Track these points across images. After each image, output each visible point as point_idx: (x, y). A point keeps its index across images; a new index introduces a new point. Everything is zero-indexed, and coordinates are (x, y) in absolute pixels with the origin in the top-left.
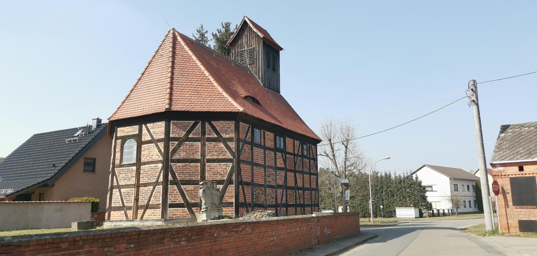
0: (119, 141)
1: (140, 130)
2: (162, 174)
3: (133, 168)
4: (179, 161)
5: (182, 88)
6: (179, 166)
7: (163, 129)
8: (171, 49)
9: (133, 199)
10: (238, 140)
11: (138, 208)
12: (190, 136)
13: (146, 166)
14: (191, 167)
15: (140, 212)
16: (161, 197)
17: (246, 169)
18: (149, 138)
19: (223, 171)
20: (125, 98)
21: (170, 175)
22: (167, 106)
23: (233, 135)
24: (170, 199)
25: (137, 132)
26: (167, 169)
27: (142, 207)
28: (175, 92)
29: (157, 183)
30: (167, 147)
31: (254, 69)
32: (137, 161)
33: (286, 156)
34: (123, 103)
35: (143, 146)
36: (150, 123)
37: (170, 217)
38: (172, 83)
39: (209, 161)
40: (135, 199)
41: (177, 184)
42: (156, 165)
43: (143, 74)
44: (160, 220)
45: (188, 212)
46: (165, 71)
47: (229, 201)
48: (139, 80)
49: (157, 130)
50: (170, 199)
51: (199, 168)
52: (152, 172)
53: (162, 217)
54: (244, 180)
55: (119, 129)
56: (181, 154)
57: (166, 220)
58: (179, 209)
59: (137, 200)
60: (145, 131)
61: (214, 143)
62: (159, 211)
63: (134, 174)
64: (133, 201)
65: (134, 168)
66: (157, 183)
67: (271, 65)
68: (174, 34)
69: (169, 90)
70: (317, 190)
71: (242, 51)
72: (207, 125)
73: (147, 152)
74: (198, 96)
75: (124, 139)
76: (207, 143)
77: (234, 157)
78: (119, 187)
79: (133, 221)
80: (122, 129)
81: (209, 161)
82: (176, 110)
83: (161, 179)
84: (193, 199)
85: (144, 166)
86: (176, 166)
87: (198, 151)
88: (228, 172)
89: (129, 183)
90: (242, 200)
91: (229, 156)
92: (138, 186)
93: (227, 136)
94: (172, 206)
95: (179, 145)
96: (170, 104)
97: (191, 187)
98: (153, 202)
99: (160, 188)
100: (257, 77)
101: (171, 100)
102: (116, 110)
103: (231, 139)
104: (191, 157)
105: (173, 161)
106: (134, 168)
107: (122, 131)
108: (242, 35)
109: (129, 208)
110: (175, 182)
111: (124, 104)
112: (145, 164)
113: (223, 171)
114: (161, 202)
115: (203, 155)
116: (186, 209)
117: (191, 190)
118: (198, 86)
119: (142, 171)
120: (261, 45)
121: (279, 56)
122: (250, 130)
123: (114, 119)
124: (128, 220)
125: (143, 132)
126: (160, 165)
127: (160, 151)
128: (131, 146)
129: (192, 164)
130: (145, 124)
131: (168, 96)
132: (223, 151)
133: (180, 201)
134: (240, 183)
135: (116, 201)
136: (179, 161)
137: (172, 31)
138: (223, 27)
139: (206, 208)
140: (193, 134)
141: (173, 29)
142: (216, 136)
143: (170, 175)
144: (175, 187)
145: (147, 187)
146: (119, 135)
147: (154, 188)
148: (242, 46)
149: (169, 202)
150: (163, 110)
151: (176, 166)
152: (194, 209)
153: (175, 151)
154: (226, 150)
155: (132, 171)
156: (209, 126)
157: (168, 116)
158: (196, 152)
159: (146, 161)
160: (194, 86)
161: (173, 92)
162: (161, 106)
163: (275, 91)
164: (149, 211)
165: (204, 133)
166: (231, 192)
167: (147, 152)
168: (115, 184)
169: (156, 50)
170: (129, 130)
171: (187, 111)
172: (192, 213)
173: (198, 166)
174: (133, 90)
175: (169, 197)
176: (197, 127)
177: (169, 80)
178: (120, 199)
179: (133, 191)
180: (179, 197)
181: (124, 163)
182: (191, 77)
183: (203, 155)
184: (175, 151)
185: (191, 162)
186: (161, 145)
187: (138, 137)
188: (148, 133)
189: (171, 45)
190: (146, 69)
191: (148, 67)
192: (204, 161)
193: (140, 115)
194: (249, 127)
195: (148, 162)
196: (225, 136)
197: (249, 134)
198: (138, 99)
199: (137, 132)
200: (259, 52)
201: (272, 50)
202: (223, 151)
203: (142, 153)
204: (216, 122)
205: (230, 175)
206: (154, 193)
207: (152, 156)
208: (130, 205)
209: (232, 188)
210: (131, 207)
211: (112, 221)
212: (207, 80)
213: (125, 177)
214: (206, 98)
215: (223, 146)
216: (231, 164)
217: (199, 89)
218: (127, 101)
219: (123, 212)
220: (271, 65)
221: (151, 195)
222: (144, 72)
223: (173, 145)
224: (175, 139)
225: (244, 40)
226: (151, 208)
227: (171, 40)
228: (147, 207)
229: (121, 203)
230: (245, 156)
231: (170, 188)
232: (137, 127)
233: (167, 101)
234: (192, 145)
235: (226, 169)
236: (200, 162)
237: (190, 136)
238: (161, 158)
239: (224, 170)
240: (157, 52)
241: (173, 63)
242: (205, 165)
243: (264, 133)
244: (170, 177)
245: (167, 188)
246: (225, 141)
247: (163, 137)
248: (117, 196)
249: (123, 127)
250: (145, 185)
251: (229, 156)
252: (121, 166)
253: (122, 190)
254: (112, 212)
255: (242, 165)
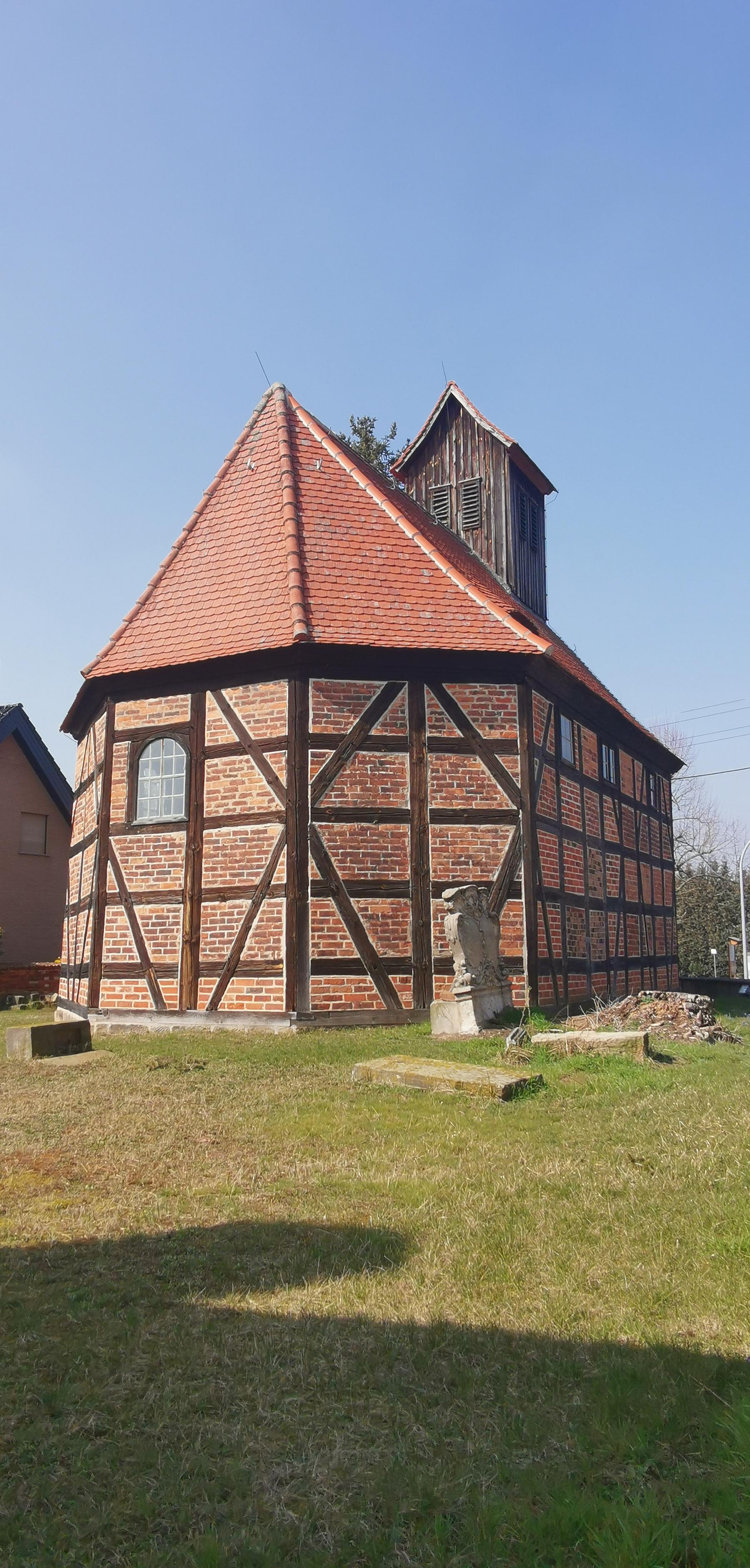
0: (122, 747)
1: (199, 710)
2: (283, 859)
3: (174, 835)
4: (340, 815)
5: (337, 572)
6: (342, 834)
7: (283, 707)
8: (283, 450)
9: (180, 940)
10: (531, 750)
11: (196, 970)
12: (373, 732)
13: (224, 830)
14: (382, 835)
15: (208, 985)
16: (283, 938)
17: (547, 839)
18: (231, 737)
19: (487, 851)
20: (134, 606)
21: (312, 863)
22: (299, 629)
23: (514, 732)
24: (315, 945)
25: (188, 718)
26: (299, 840)
27: (212, 968)
28: (316, 585)
29: (265, 889)
30: (298, 769)
31: (482, 543)
32: (188, 812)
33: (620, 807)
34: (131, 621)
35: (208, 762)
36: (234, 684)
37: (315, 1007)
38: (301, 555)
39: (440, 816)
40: (185, 942)
41: (335, 893)
42: (261, 827)
43: (190, 530)
44: (283, 1016)
45: (375, 991)
46: (270, 517)
47: (509, 952)
48: (180, 547)
49: (259, 710)
50: (315, 945)
51: (407, 840)
52: (246, 849)
53: (291, 1005)
54: (550, 882)
55: (120, 706)
56: (347, 793)
57: (303, 1017)
58: (345, 977)
59: (192, 943)
60: (213, 712)
61: (453, 758)
62: (278, 985)
63: (180, 856)
64: (179, 947)
65: (180, 836)
66: (265, 889)
67: (528, 535)
68: (286, 403)
69: (293, 576)
70: (671, 912)
71: (442, 490)
72: (429, 696)
73: (225, 782)
74: (391, 598)
75: (141, 739)
76: (430, 757)
77: (521, 805)
78: (127, 899)
79: (181, 1013)
80: (131, 705)
81: (440, 816)
82: (329, 641)
83: (281, 876)
84: (388, 946)
85: (214, 831)
86: (329, 833)
87: (404, 784)
88: (503, 854)
89: (161, 887)
90: (542, 950)
91: (503, 800)
92: (195, 896)
93: (496, 735)
94: (323, 967)
95: (339, 762)
96: (307, 622)
97: (381, 905)
98: (251, 950)
99: (278, 906)
100: (492, 569)
101: (306, 608)
102: (109, 643)
103: (507, 746)
104: (380, 803)
105: (319, 815)
106: (180, 836)
107: (132, 714)
108: (442, 441)
109: (168, 971)
110: (328, 886)
111: (136, 624)
112: (218, 822)
113: (487, 851)
114: (283, 955)
115: (419, 798)
116: (369, 978)
117: (384, 916)
118: (386, 569)
119: (207, 848)
120: (505, 470)
121: (544, 510)
122: (552, 717)
123: (108, 673)
124: (162, 1009)
125: (209, 717)
126: (276, 829)
127: (273, 781)
128: (164, 764)
129: (382, 827)
130: (216, 690)
131: (294, 597)
132: (482, 786)
133: (344, 952)
134: (539, 894)
135: (119, 946)
136: (340, 815)
137: (278, 395)
138: (355, 431)
139: (473, 982)
140: (384, 725)
141: (283, 389)
142: (459, 733)
143: (312, 863)
144: (331, 903)
145: (229, 903)
146: (119, 726)
147: (256, 905)
148: (440, 474)
149: (312, 954)
150: (287, 641)
151: (329, 833)
152: (395, 979)
153: (325, 781)
154: (494, 781)
155: (173, 845)
156: (436, 701)
157: (299, 663)
158: (396, 786)
159: (221, 812)
160: (375, 568)
161: (309, 585)
162: (280, 629)
163: (536, 612)
164: (238, 985)
165: (418, 721)
166: (513, 924)
167: (225, 782)
168: (112, 886)
169: (229, 454)
170: (158, 709)
171: (368, 647)
172: (388, 991)
173: (404, 835)
174: (160, 579)
175: (312, 938)
176: (397, 701)
177: (290, 544)
178: (131, 938)
179: (179, 912)
180: (344, 937)
181: (140, 820)
182: (361, 539)
183: (419, 798)
184: (325, 781)
185: (381, 820)
186: (278, 762)
187: (191, 734)
188: (225, 721)
189: (282, 435)
190: (201, 513)
191: (206, 506)
192: (422, 818)
193: (202, 657)
194: (550, 706)
195: (231, 817)
196: (487, 734)
197: (551, 732)
198: (183, 609)
199: (188, 718)
200: (497, 491)
201: (529, 486)
202: (482, 786)
203: (208, 786)
204: (457, 688)
205: (510, 866)
206: (255, 923)
207: (244, 796)
208: (168, 959)
209: (516, 912)
210: (175, 966)
211: (106, 1012)
212: (411, 550)
213: (151, 865)
214: (420, 608)
215: (483, 767)
216: (510, 830)
217: (391, 577)
218: (144, 616)
219: (143, 983)
220: (528, 535)
221: (246, 928)
222: (195, 523)
223: (319, 760)
224: (323, 741)
225: (448, 455)
226: (246, 974)
227: (280, 421)
228: (232, 968)
229: (136, 953)
230: (545, 805)
231: (315, 906)
232: (186, 699)
233: (296, 613)
234: (382, 763)
235: (495, 844)
236: (411, 821)
237: (373, 732)
238: (278, 805)
239: (489, 848)
240: (232, 460)
241: (296, 490)
242: (425, 831)
243: (579, 727)
244: (313, 870)
245: (305, 907)
246: (488, 751)
247: (285, 732)
248: (118, 928)
249: (136, 698)
250: (222, 895)
251: (503, 800)
252: (130, 828)
253: (136, 908)
254: (105, 983)
255: (541, 834)
